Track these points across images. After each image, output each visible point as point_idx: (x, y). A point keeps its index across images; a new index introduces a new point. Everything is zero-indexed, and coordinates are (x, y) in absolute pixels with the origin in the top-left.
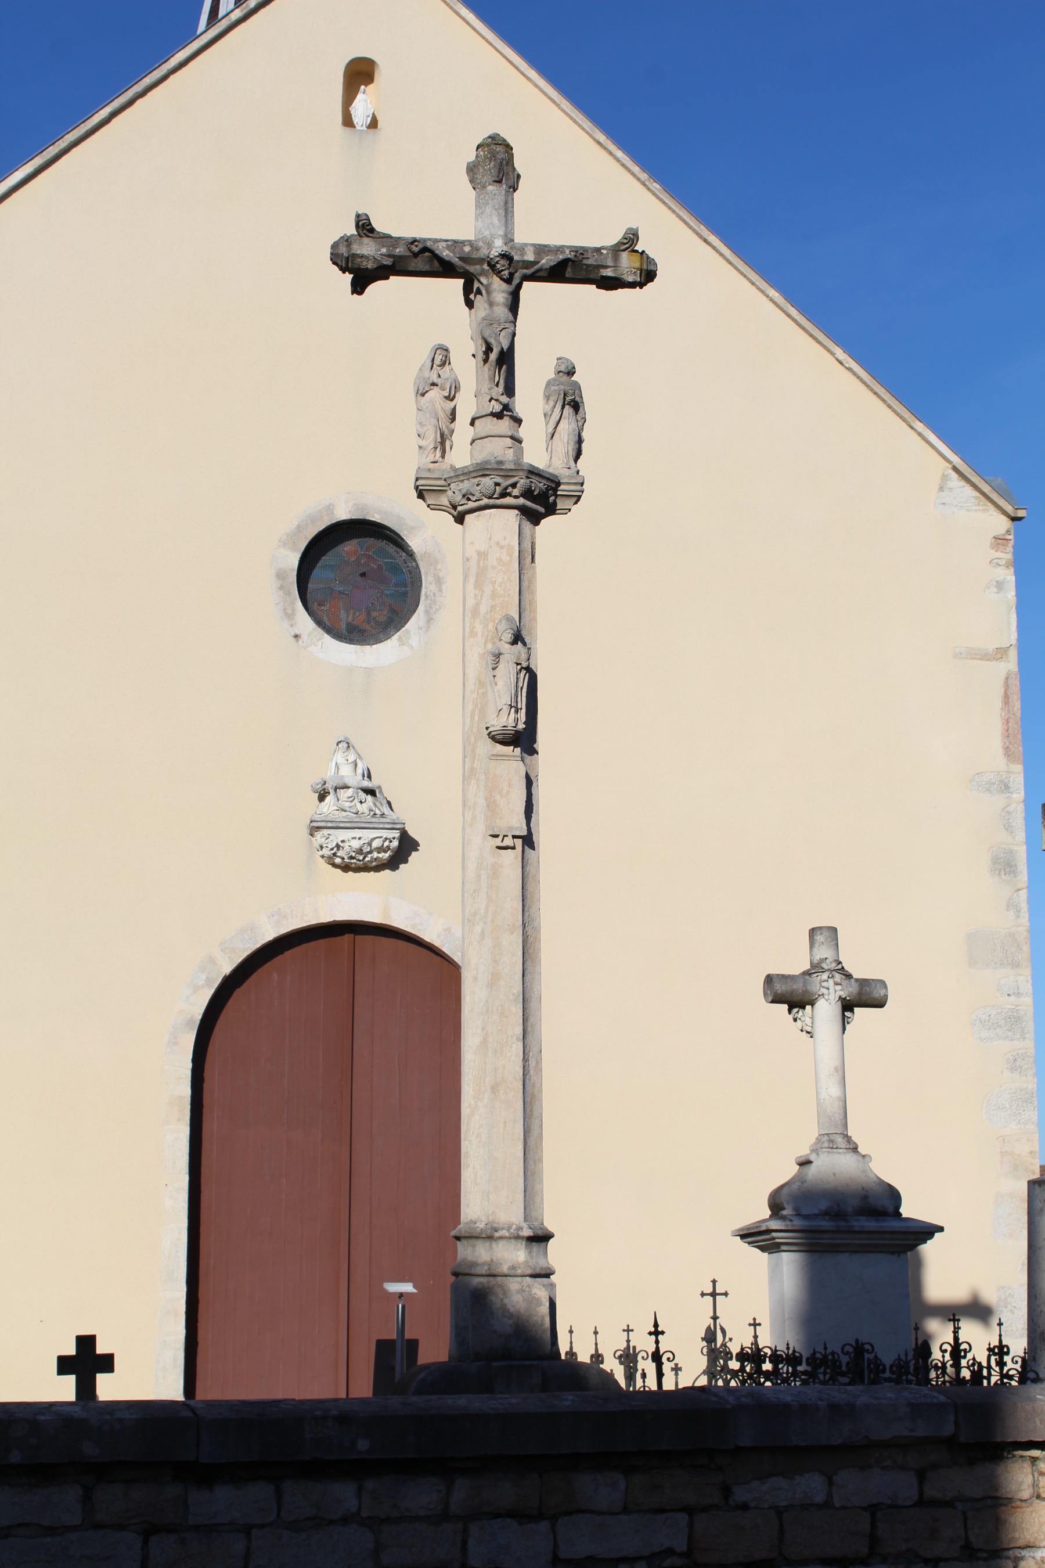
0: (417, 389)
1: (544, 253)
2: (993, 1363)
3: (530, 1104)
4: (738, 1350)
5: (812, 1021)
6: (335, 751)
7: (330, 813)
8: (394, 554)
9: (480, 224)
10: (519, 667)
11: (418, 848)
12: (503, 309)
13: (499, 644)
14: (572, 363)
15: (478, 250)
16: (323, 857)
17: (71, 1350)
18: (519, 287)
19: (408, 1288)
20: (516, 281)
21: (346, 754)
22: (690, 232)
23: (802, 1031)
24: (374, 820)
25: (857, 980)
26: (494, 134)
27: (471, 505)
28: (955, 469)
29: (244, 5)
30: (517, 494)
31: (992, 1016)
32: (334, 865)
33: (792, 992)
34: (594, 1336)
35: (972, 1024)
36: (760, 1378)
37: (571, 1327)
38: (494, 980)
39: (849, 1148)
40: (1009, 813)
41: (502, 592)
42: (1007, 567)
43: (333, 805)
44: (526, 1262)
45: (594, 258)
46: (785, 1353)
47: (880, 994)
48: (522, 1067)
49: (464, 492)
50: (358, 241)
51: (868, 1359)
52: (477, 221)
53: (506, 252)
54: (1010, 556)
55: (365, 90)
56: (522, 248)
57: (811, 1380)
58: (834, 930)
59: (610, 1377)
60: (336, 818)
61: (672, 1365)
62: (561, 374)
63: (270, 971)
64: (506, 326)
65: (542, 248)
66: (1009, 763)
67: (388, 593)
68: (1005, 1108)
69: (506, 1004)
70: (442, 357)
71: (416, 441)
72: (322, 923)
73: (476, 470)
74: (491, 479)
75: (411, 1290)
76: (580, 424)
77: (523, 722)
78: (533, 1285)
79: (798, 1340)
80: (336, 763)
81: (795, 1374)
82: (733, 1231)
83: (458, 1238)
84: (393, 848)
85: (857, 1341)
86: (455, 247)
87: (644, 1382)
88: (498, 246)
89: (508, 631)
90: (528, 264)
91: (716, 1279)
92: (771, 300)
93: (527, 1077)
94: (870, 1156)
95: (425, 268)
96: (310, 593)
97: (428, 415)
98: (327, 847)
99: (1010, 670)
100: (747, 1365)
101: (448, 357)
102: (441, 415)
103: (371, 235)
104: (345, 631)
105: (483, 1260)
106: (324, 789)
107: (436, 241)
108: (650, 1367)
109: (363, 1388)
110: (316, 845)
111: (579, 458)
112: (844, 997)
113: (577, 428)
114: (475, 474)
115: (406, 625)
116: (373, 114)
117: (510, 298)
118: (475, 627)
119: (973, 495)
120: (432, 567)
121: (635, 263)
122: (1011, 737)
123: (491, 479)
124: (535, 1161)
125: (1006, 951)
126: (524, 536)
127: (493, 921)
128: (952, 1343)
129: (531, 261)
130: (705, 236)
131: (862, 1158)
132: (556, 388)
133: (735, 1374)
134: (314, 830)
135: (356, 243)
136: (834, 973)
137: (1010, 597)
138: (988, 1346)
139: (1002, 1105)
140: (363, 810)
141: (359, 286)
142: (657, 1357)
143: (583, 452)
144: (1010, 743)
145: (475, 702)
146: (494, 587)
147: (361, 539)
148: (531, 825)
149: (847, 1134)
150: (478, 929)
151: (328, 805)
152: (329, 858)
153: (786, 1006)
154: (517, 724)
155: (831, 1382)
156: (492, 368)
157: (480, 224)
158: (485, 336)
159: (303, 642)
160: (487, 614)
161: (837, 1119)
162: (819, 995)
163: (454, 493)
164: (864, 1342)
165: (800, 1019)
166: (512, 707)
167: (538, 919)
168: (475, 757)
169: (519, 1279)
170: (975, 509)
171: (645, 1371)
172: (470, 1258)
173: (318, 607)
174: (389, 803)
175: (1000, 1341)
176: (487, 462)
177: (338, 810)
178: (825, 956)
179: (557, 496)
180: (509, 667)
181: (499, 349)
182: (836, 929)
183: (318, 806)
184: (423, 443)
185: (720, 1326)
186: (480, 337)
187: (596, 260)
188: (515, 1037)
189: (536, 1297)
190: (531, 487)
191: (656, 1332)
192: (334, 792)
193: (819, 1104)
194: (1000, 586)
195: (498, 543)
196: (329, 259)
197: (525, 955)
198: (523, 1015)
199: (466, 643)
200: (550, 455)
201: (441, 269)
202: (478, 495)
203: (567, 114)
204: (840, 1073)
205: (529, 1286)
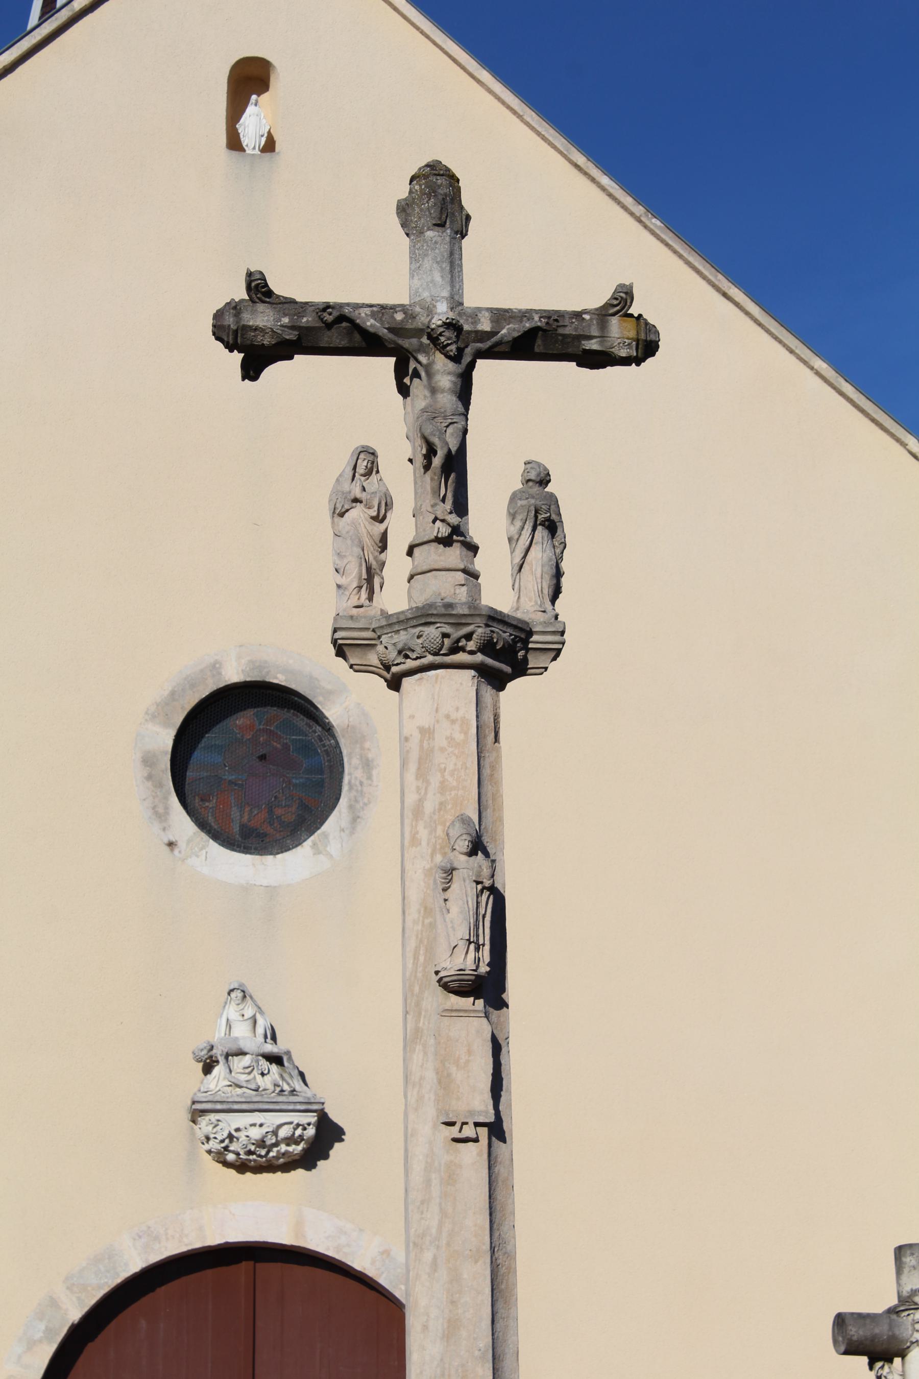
1: (505, 320)
6: (226, 1003)
7: (219, 1090)
10: (480, 887)
11: (343, 1137)
12: (449, 397)
13: (451, 855)
14: (546, 469)
15: (414, 318)
16: (209, 1152)
18: (471, 366)
20: (467, 359)
21: (241, 1007)
22: (703, 283)
24: (280, 1099)
26: (433, 161)
27: (410, 664)
30: (474, 648)
32: (226, 1164)
33: (873, 1338)
38: (452, 1329)
41: (455, 784)
43: (225, 1078)
45: (573, 325)
49: (400, 646)
50: (249, 309)
52: (413, 279)
53: (453, 319)
56: (474, 314)
60: (228, 1097)
62: (531, 484)
67: (298, 782)
69: (470, 1364)
72: (210, 1247)
74: (437, 628)
76: (558, 551)
77: (486, 963)
80: (228, 1020)
84: (309, 1138)
88: (442, 312)
89: (465, 837)
92: (818, 373)
95: (343, 343)
96: (189, 784)
97: (349, 542)
98: (215, 1138)
101: (375, 463)
102: (367, 541)
103: (268, 300)
104: (237, 836)
106: (211, 1057)
107: (357, 306)
110: (200, 1135)
113: (554, 557)
114: (415, 622)
116: (269, 133)
117: (459, 382)
118: (417, 833)
120: (358, 746)
123: (437, 628)
126: (484, 705)
127: (448, 1244)
129: (486, 331)
132: (524, 502)
134: (196, 1114)
140: (266, 1085)
143: (563, 589)
146: (443, 776)
147: (259, 709)
150: (428, 1256)
151: (217, 1078)
153: (865, 1360)
154: (478, 967)
156: (436, 477)
158: (426, 434)
159: (180, 852)
160: (434, 813)
162: (912, 1343)
163: (386, 648)
166: (470, 943)
168: (420, 1014)
173: (201, 803)
174: (302, 1075)
176: (431, 606)
179: (528, 650)
181: (445, 451)
184: (342, 581)
186: (419, 435)
187: (576, 329)
190: (492, 638)
192: (224, 1061)
195: (447, 717)
196: (211, 333)
197: (495, 1292)
201: (364, 344)
202: (419, 651)
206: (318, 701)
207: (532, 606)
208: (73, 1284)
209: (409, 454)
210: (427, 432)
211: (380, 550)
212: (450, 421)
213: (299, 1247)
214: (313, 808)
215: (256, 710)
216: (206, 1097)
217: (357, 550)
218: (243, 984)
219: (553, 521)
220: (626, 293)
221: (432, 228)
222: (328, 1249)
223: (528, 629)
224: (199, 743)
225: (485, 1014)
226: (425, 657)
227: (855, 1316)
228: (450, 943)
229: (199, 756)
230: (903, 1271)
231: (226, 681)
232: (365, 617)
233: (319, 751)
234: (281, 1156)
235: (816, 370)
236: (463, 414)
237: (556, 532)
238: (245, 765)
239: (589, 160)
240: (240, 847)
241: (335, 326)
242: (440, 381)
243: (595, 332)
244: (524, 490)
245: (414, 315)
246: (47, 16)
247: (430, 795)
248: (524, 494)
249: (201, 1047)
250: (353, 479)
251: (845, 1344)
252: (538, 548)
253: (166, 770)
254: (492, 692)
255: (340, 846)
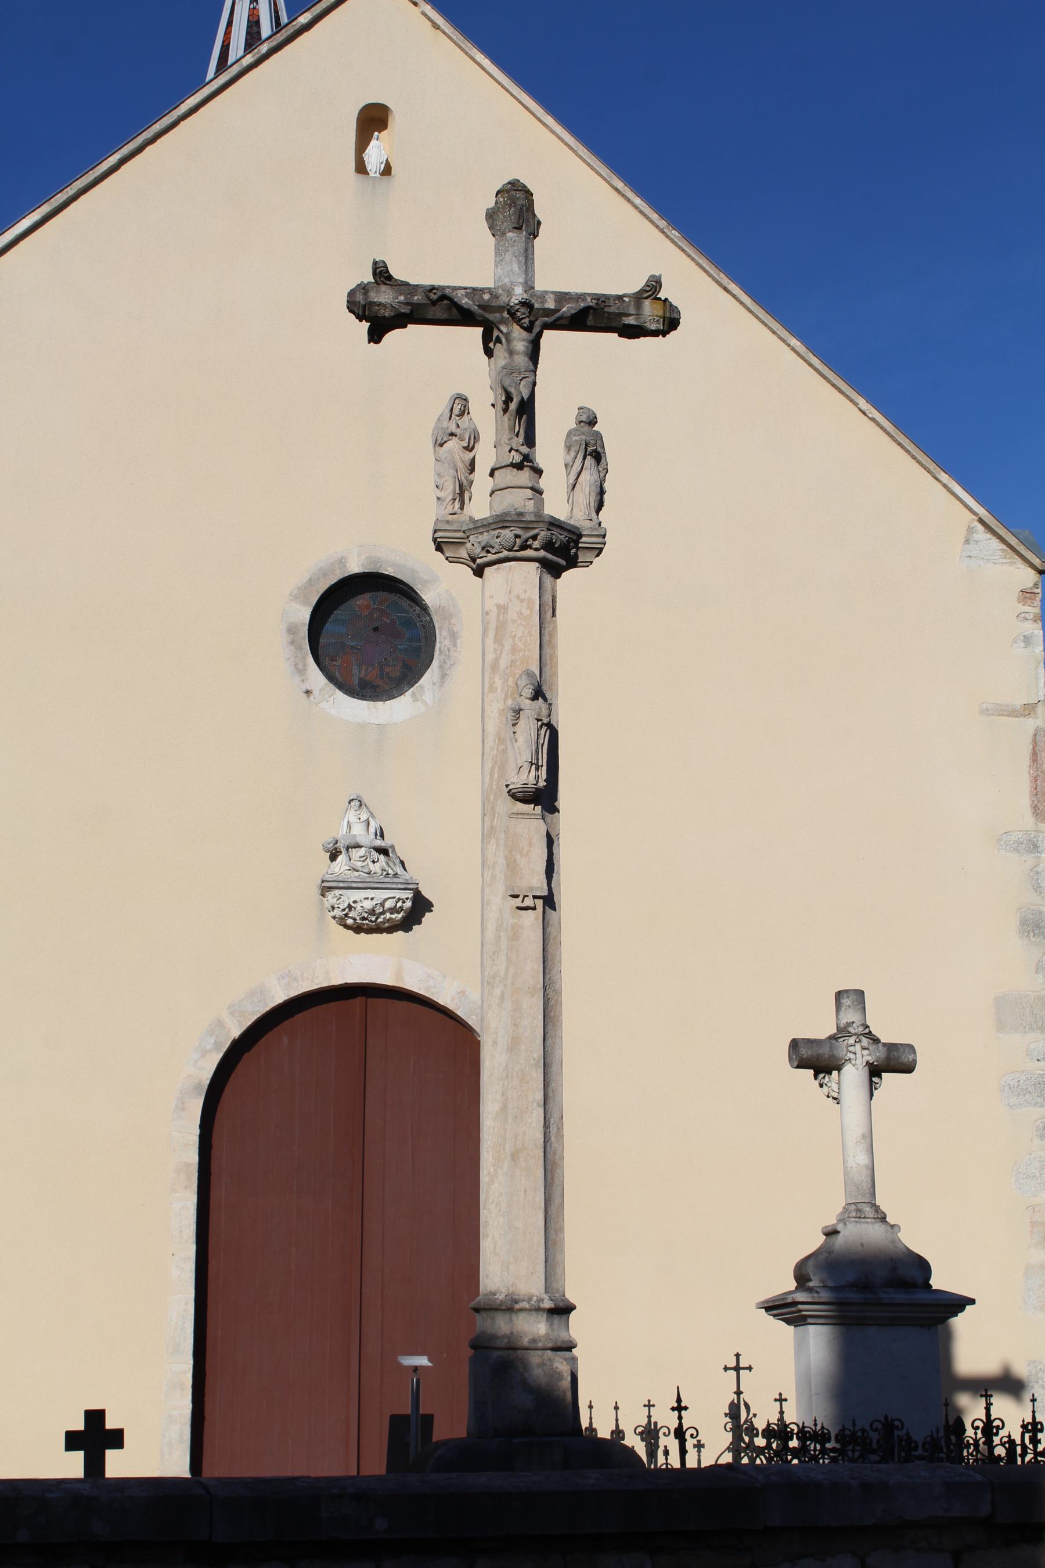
0: (435, 439)
1: (565, 300)
2: (1027, 1441)
3: (551, 1172)
4: (764, 1426)
5: (839, 1086)
6: (347, 809)
7: (342, 873)
8: (408, 608)
9: (499, 271)
10: (540, 723)
11: (432, 908)
12: (523, 358)
13: (519, 699)
14: (594, 413)
15: (498, 298)
16: (334, 917)
17: (79, 1425)
18: (539, 335)
19: (423, 1361)
20: (536, 330)
21: (358, 812)
22: (710, 280)
23: (828, 1097)
24: (386, 880)
25: (885, 1044)
26: (513, 180)
27: (491, 557)
28: (981, 521)
29: (256, 50)
30: (538, 546)
31: (1022, 1082)
32: (346, 927)
33: (818, 1056)
34: (615, 1411)
35: (1000, 1090)
36: (787, 1455)
37: (591, 1402)
38: (514, 1044)
39: (878, 1218)
40: (1038, 873)
41: (522, 647)
42: (1035, 621)
43: (346, 864)
44: (547, 1335)
45: (616, 306)
46: (812, 1429)
47: (909, 1059)
48: (543, 1134)
49: (483, 544)
50: (375, 289)
51: (899, 1436)
52: (497, 268)
53: (527, 299)
54: (1037, 610)
55: (378, 136)
56: (543, 296)
57: (840, 1458)
58: (860, 994)
59: (631, 1451)
60: (348, 878)
61: (695, 1441)
62: (582, 424)
63: (279, 1037)
64: (526, 376)
65: (563, 295)
66: (1037, 822)
67: (402, 647)
68: (1035, 1176)
69: (527, 1069)
70: (461, 406)
71: (433, 493)
72: (334, 986)
73: (495, 522)
74: (511, 530)
75: (426, 1363)
76: (602, 475)
77: (544, 779)
78: (555, 1359)
79: (825, 1416)
80: (348, 822)
81: (824, 1451)
82: (758, 1304)
83: (477, 1310)
84: (406, 909)
85: (886, 1417)
86: (474, 294)
87: (667, 1459)
88: (519, 293)
89: (529, 686)
90: (548, 312)
91: (740, 1353)
92: (793, 349)
93: (548, 1144)
94: (898, 1226)
95: (444, 316)
96: (321, 648)
97: (446, 465)
98: (338, 907)
99: (1038, 727)
100: (774, 1442)
101: (467, 406)
102: (460, 465)
103: (389, 283)
104: (357, 687)
105: (503, 1333)
106: (336, 849)
108: (673, 1445)
109: (376, 1464)
110: (327, 905)
111: (601, 509)
112: (871, 1062)
113: (599, 479)
114: (495, 526)
115: (420, 681)
116: (387, 161)
117: (530, 346)
118: (494, 683)
119: (1000, 548)
120: (447, 621)
121: (658, 311)
122: (1039, 796)
123: (511, 530)
124: (556, 1231)
125: (1036, 1014)
126: (545, 589)
127: (512, 983)
128: (985, 1421)
129: (551, 309)
130: (725, 285)
131: (890, 1227)
132: (577, 438)
133: (760, 1451)
134: (325, 890)
135: (373, 290)
136: (861, 1037)
137: (1038, 652)
138: (1022, 1423)
139: (1032, 1173)
140: (376, 870)
141: (376, 335)
142: (680, 1434)
143: (605, 503)
144: (1038, 801)
145: (495, 758)
146: (514, 641)
147: (374, 593)
148: (552, 885)
149: (875, 1203)
150: (497, 991)
151: (340, 864)
152: (341, 918)
153: (811, 1072)
154: (537, 782)
155: (861, 1460)
156: (512, 418)
157: (499, 271)
158: (505, 386)
159: (314, 698)
160: (507, 669)
161: (865, 1188)
162: (846, 1060)
163: (473, 545)
164: (894, 1418)
165: (826, 1085)
166: (532, 764)
167: (559, 981)
168: (494, 815)
169: (540, 1352)
170: (1001, 561)
171: (668, 1448)
172: (489, 1331)
173: (330, 662)
174: (402, 863)
175: (1034, 1417)
176: (507, 514)
177: (350, 870)
178: (852, 1020)
179: (578, 548)
180: (529, 723)
181: (519, 398)
182: (862, 992)
183: (330, 865)
184: (441, 494)
185: (744, 1401)
186: (500, 386)
187: (618, 308)
188: (535, 1103)
189: (558, 1371)
190: (552, 539)
191: (679, 1408)
192: (346, 852)
193: (846, 1172)
194: (1027, 640)
195: (518, 597)
196: (346, 307)
197: (546, 1018)
198: (544, 1080)
199: (485, 699)
200: (571, 507)
201: (459, 317)
202: (497, 547)
203: (584, 161)
204: (868, 1140)
205: (549, 1359)
206: (418, 588)
207: (582, 515)
208: (235, 1011)
209: (492, 401)
210: (506, 384)
211: (469, 472)
212: (523, 376)
213: (399, 987)
214: (413, 667)
215: (371, 594)
216: (332, 878)
217: (452, 472)
218: (360, 796)
219: (599, 452)
220: (656, 282)
221: (512, 230)
222: (420, 989)
223: (579, 533)
224: (329, 617)
225: (542, 816)
226: (502, 552)
227: (806, 1041)
228: (517, 764)
229: (329, 627)
230: (841, 1009)
231: (349, 572)
232: (458, 522)
233: (418, 625)
234: (386, 921)
235: (792, 347)
236: (533, 371)
237: (601, 460)
238: (363, 635)
239: (626, 185)
240: (359, 695)
241: (438, 303)
242: (516, 346)
243: (632, 311)
244: (577, 428)
245: (497, 296)
246: (220, 72)
247: (504, 655)
248: (577, 432)
249: (329, 841)
250: (450, 419)
251: (798, 1061)
252: (587, 472)
253: (305, 637)
254: (551, 579)
255: (432, 695)
